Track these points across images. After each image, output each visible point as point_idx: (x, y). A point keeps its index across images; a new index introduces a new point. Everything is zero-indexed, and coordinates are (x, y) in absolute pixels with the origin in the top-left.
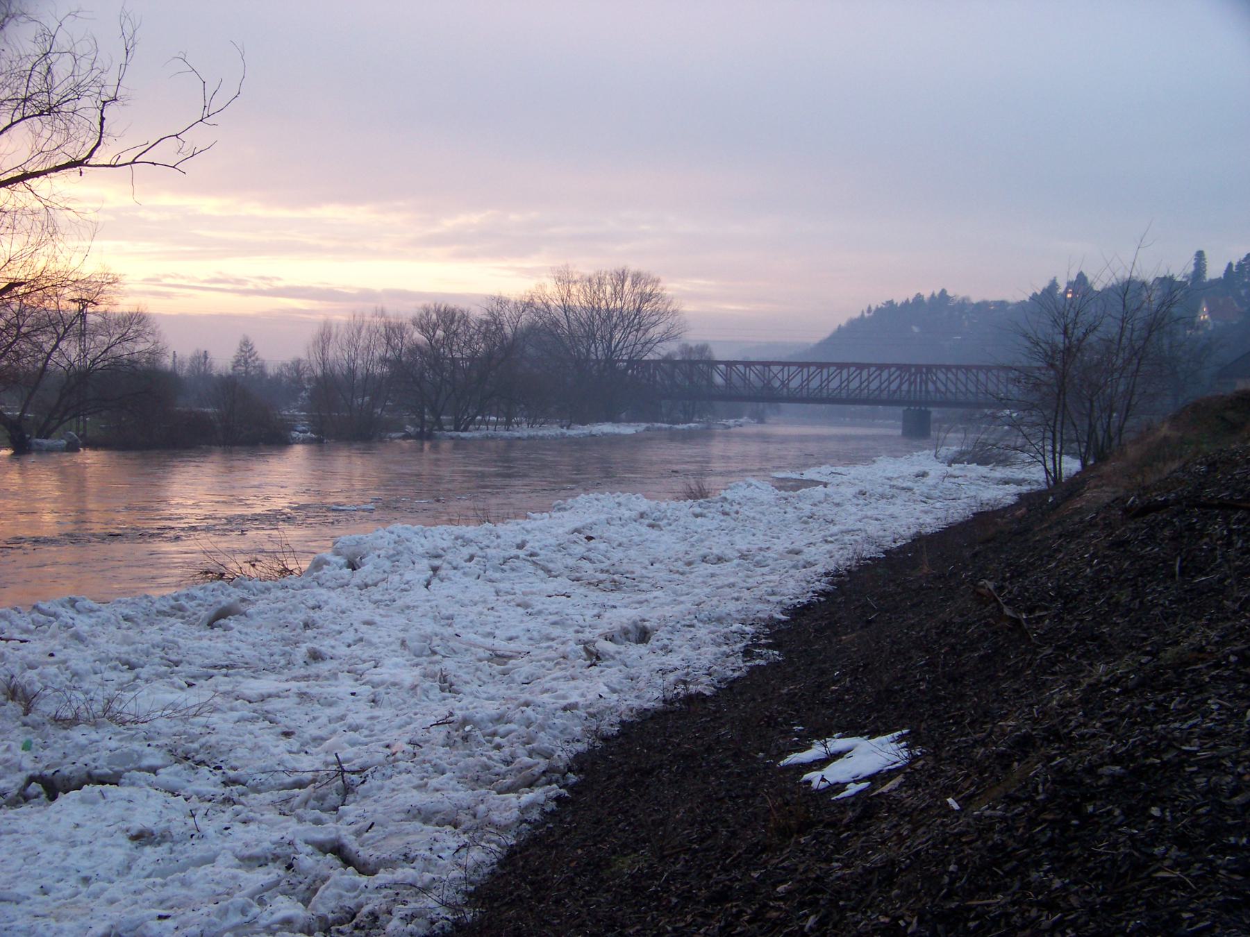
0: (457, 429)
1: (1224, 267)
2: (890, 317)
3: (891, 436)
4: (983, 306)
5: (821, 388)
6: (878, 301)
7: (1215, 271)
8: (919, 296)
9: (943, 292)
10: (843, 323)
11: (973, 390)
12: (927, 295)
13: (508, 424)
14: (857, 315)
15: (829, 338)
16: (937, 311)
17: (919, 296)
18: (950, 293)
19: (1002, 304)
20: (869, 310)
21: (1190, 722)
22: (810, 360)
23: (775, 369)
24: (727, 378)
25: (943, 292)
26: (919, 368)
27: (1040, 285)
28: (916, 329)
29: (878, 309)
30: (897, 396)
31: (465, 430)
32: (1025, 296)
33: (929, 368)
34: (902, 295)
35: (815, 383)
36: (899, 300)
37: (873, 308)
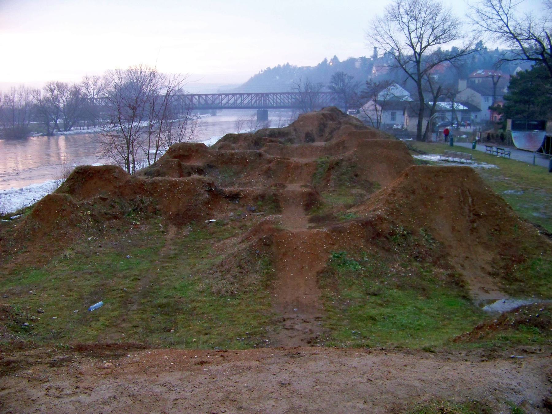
0: (66, 130)
1: (323, 60)
2: (270, 73)
3: (229, 122)
4: (301, 69)
5: (241, 103)
6: (265, 68)
7: (381, 53)
8: (279, 65)
9: (288, 63)
10: (253, 76)
11: (279, 102)
12: (282, 65)
13: (510, 285)
14: (257, 73)
15: (248, 82)
16: (284, 71)
17: (279, 65)
18: (290, 64)
19: (308, 68)
20: (262, 71)
21: (315, 230)
22: (236, 92)
23: (209, 96)
24: (199, 101)
25: (288, 63)
26: (263, 94)
27: (277, 66)
28: (277, 77)
29: (265, 71)
30: (255, 105)
31: (69, 130)
32: (299, 66)
33: (267, 94)
34: (273, 65)
35: (239, 101)
36: (272, 67)
37: (263, 70)
